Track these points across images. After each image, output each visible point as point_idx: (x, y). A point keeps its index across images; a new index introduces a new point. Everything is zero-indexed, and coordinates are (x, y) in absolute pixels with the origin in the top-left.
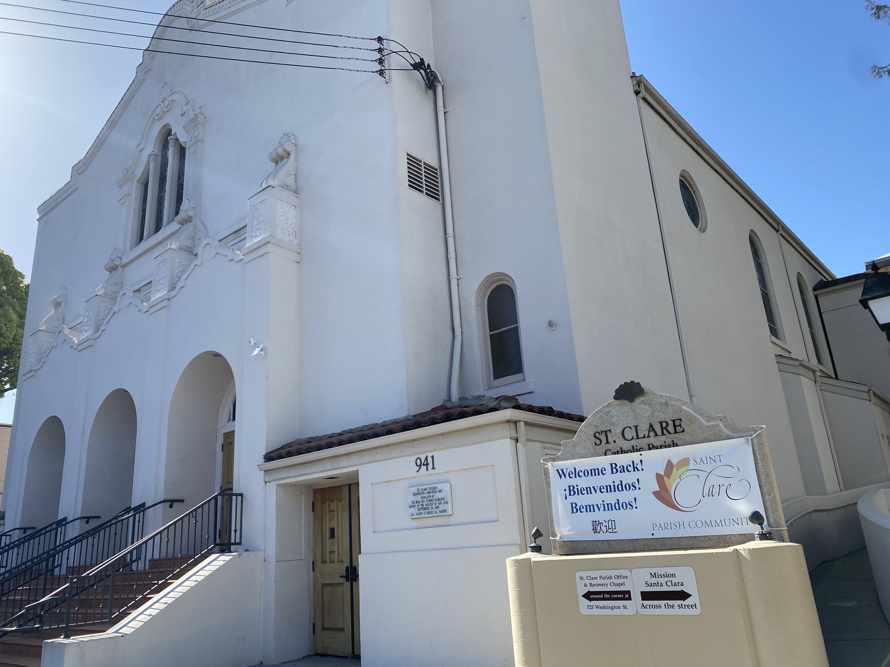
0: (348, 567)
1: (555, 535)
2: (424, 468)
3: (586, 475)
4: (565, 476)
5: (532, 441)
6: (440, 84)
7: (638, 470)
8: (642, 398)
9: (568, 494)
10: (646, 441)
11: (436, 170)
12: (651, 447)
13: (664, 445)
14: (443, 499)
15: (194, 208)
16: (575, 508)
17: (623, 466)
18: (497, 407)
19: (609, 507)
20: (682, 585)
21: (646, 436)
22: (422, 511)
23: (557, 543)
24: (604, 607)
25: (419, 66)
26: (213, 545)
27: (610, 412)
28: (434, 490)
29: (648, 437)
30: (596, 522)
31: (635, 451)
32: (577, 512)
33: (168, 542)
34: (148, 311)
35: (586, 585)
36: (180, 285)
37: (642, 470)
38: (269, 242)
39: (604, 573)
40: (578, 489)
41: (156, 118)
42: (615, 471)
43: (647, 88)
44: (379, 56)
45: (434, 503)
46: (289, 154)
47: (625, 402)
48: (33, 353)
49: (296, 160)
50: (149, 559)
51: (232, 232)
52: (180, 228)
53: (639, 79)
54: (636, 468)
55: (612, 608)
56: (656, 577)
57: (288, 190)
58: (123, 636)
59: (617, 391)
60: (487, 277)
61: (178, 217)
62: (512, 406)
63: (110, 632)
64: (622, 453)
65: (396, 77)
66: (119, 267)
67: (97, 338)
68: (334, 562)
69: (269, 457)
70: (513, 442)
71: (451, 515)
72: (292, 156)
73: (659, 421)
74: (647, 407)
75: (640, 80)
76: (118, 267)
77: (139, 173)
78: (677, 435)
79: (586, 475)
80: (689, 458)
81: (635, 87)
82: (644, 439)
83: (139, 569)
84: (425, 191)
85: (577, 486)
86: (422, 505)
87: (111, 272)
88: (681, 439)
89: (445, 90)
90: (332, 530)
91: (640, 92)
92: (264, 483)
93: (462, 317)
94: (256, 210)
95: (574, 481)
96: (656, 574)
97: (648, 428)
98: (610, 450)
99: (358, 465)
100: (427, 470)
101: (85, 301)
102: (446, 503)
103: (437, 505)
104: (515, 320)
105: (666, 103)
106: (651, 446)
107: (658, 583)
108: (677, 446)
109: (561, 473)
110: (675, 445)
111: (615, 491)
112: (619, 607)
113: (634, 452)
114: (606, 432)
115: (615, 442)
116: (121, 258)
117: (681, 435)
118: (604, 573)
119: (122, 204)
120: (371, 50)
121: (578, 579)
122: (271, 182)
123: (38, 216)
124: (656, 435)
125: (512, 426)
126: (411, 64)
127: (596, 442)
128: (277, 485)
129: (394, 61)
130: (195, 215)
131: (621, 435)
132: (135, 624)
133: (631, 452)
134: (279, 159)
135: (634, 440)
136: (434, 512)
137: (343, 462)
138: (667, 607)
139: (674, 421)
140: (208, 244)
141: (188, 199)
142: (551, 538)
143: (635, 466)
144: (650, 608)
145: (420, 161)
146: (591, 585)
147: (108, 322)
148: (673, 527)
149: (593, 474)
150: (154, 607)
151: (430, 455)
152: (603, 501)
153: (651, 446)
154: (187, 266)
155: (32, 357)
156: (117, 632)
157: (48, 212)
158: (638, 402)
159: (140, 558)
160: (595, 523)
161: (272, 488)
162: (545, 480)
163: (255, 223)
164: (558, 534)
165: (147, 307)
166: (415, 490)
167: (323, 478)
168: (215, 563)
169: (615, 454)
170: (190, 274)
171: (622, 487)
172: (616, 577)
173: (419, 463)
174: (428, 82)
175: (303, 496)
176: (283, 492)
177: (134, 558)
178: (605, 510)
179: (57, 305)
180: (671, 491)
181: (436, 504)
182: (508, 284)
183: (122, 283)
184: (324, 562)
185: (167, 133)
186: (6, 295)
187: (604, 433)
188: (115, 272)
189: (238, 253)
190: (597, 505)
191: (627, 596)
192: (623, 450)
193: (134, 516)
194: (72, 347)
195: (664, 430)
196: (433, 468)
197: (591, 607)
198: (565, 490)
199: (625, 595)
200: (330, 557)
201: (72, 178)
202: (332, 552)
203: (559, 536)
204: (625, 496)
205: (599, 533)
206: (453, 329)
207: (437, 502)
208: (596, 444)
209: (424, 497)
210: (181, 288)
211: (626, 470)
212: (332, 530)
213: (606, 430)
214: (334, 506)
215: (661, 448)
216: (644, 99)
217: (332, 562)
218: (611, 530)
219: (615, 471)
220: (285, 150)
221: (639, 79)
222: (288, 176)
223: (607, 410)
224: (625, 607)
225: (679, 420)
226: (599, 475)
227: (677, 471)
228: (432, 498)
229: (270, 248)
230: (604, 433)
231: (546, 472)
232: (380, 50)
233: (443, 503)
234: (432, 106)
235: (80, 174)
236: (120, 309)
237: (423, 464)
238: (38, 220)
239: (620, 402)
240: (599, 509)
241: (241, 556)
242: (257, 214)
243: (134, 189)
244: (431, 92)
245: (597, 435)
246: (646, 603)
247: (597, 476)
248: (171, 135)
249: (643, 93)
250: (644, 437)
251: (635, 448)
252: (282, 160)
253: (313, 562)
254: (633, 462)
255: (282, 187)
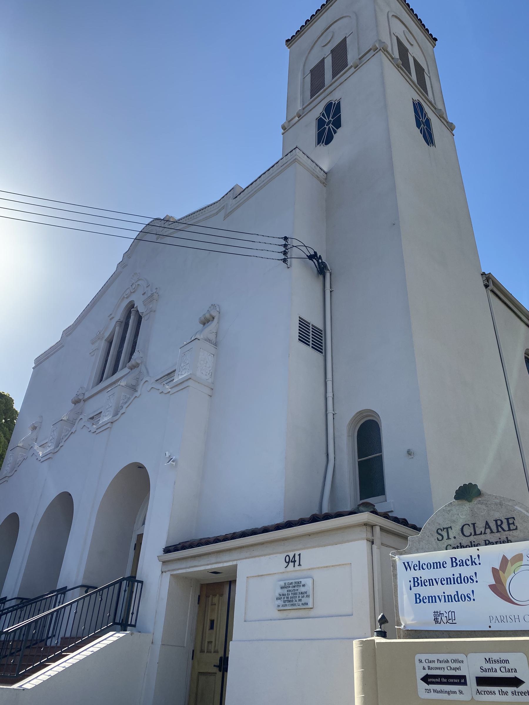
0: (222, 657)
1: (399, 624)
2: (291, 564)
3: (429, 568)
4: (410, 568)
5: (387, 546)
6: (328, 271)
7: (476, 564)
8: (480, 499)
9: (412, 585)
10: (483, 537)
11: (322, 331)
12: (488, 543)
13: (499, 541)
14: (306, 592)
15: (142, 358)
16: (418, 599)
17: (462, 560)
18: (356, 511)
19: (449, 598)
20: (516, 671)
21: (483, 533)
22: (286, 603)
23: (402, 633)
24: (441, 692)
25: (313, 257)
26: (112, 623)
27: (451, 511)
28: (298, 584)
29: (485, 533)
30: (437, 612)
31: (473, 546)
32: (420, 602)
33: (76, 613)
34: (95, 431)
35: (424, 669)
36: (122, 411)
37: (480, 564)
38: (190, 378)
39: (442, 657)
40: (421, 581)
41: (125, 297)
42: (454, 564)
43: (495, 283)
44: (284, 249)
45: (297, 596)
46: (214, 318)
47: (465, 502)
48: (10, 463)
49: (218, 323)
50: (61, 637)
51: (165, 374)
52: (129, 372)
53: (488, 276)
54: (474, 562)
55: (449, 693)
56: (490, 663)
57: (209, 342)
58: (24, 690)
59: (457, 492)
60: (357, 413)
61: (130, 364)
62: (370, 511)
63: (16, 686)
64: (461, 548)
65: (295, 263)
66: (82, 400)
67: (56, 452)
68: (211, 652)
69: (167, 550)
70: (370, 543)
71: (312, 608)
72: (216, 320)
73: (495, 519)
74: (484, 507)
75: (489, 276)
76: (81, 401)
77: (107, 334)
78: (511, 532)
79: (429, 568)
80: (522, 554)
81: (484, 281)
82: (481, 535)
83: (52, 645)
84: (311, 345)
85: (421, 578)
86: (287, 598)
87: (75, 404)
88: (514, 536)
89: (332, 276)
90: (212, 622)
91: (489, 286)
92: (161, 572)
93: (336, 445)
94: (184, 356)
95: (418, 574)
96: (491, 659)
97: (485, 525)
98: (451, 545)
99: (237, 560)
100: (294, 566)
101: (53, 424)
102: (308, 596)
103: (300, 598)
104: (380, 451)
105: (511, 296)
106: (487, 542)
107: (492, 669)
108: (511, 542)
109: (407, 566)
110: (508, 541)
111: (454, 583)
112: (455, 692)
113: (472, 547)
114: (447, 528)
115: (455, 538)
116: (84, 394)
117: (515, 533)
118: (442, 657)
119: (92, 356)
120: (278, 245)
121: (417, 662)
122: (198, 336)
123: (34, 365)
124: (492, 532)
125: (369, 529)
126: (307, 256)
127: (439, 538)
128: (171, 575)
129: (294, 252)
130: (141, 363)
131: (460, 532)
132: (36, 682)
133: (470, 547)
134: (206, 322)
135: (472, 536)
136: (297, 605)
137: (225, 557)
138: (501, 693)
139: (507, 519)
140: (147, 381)
141: (139, 351)
142: (396, 627)
143: (473, 560)
144: (485, 694)
145: (309, 324)
146: (429, 669)
147: (66, 440)
148: (509, 619)
149: (435, 567)
150: (53, 669)
151: (297, 553)
152: (444, 593)
153: (487, 542)
154: (129, 398)
155: (8, 467)
156: (21, 686)
157: (41, 363)
158: (475, 502)
159: (54, 636)
160: (436, 613)
161: (167, 577)
162: (393, 572)
163: (182, 365)
164: (402, 623)
165: (95, 428)
166: (282, 583)
167: (207, 571)
168: (111, 638)
169: (455, 549)
170: (130, 404)
171: (460, 580)
172: (453, 661)
173: (287, 560)
174: (320, 270)
175: (192, 589)
176: (175, 582)
177: (50, 635)
178: (445, 601)
179: (34, 428)
180: (506, 585)
181: (299, 597)
182: (374, 419)
183: (81, 413)
184: (202, 651)
185: (131, 306)
186: (3, 426)
187: (446, 529)
188: (78, 404)
189: (168, 387)
190: (438, 596)
191: (463, 681)
192: (462, 545)
193: (57, 595)
194: (37, 459)
195: (499, 528)
196: (300, 565)
197: (428, 691)
198: (410, 581)
199: (461, 680)
200: (208, 646)
201: (62, 339)
202: (210, 642)
203: (403, 624)
204: (464, 589)
205: (440, 623)
206: (328, 455)
207: (300, 595)
208: (438, 540)
209: (290, 591)
210: (122, 414)
211: (464, 564)
212: (212, 622)
213: (447, 527)
214: (216, 600)
215: (496, 544)
216: (492, 291)
217: (209, 652)
218: (450, 621)
219: (454, 564)
220: (211, 315)
221: (487, 276)
222: (211, 333)
223: (449, 509)
224: (461, 692)
225: (513, 519)
226: (440, 568)
227: (512, 566)
228: (296, 592)
229: (190, 383)
230: (445, 530)
231: (394, 565)
232: (285, 246)
233: (305, 596)
234: (322, 287)
235: (67, 336)
236: (76, 430)
237: (291, 561)
238: (33, 368)
239: (460, 502)
240: (440, 601)
241: (133, 635)
242: (185, 358)
243: (102, 345)
244: (321, 277)
245: (440, 531)
246: (481, 688)
247: (439, 569)
248: (134, 308)
249: (491, 286)
250: (481, 534)
251: (473, 543)
252: (208, 322)
253: (193, 651)
254: (471, 556)
255: (205, 340)
